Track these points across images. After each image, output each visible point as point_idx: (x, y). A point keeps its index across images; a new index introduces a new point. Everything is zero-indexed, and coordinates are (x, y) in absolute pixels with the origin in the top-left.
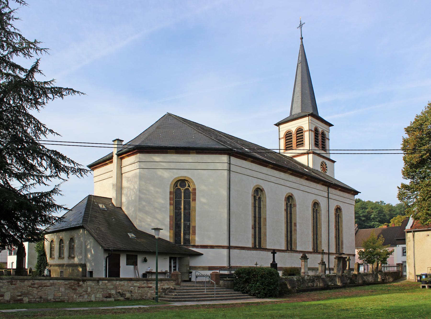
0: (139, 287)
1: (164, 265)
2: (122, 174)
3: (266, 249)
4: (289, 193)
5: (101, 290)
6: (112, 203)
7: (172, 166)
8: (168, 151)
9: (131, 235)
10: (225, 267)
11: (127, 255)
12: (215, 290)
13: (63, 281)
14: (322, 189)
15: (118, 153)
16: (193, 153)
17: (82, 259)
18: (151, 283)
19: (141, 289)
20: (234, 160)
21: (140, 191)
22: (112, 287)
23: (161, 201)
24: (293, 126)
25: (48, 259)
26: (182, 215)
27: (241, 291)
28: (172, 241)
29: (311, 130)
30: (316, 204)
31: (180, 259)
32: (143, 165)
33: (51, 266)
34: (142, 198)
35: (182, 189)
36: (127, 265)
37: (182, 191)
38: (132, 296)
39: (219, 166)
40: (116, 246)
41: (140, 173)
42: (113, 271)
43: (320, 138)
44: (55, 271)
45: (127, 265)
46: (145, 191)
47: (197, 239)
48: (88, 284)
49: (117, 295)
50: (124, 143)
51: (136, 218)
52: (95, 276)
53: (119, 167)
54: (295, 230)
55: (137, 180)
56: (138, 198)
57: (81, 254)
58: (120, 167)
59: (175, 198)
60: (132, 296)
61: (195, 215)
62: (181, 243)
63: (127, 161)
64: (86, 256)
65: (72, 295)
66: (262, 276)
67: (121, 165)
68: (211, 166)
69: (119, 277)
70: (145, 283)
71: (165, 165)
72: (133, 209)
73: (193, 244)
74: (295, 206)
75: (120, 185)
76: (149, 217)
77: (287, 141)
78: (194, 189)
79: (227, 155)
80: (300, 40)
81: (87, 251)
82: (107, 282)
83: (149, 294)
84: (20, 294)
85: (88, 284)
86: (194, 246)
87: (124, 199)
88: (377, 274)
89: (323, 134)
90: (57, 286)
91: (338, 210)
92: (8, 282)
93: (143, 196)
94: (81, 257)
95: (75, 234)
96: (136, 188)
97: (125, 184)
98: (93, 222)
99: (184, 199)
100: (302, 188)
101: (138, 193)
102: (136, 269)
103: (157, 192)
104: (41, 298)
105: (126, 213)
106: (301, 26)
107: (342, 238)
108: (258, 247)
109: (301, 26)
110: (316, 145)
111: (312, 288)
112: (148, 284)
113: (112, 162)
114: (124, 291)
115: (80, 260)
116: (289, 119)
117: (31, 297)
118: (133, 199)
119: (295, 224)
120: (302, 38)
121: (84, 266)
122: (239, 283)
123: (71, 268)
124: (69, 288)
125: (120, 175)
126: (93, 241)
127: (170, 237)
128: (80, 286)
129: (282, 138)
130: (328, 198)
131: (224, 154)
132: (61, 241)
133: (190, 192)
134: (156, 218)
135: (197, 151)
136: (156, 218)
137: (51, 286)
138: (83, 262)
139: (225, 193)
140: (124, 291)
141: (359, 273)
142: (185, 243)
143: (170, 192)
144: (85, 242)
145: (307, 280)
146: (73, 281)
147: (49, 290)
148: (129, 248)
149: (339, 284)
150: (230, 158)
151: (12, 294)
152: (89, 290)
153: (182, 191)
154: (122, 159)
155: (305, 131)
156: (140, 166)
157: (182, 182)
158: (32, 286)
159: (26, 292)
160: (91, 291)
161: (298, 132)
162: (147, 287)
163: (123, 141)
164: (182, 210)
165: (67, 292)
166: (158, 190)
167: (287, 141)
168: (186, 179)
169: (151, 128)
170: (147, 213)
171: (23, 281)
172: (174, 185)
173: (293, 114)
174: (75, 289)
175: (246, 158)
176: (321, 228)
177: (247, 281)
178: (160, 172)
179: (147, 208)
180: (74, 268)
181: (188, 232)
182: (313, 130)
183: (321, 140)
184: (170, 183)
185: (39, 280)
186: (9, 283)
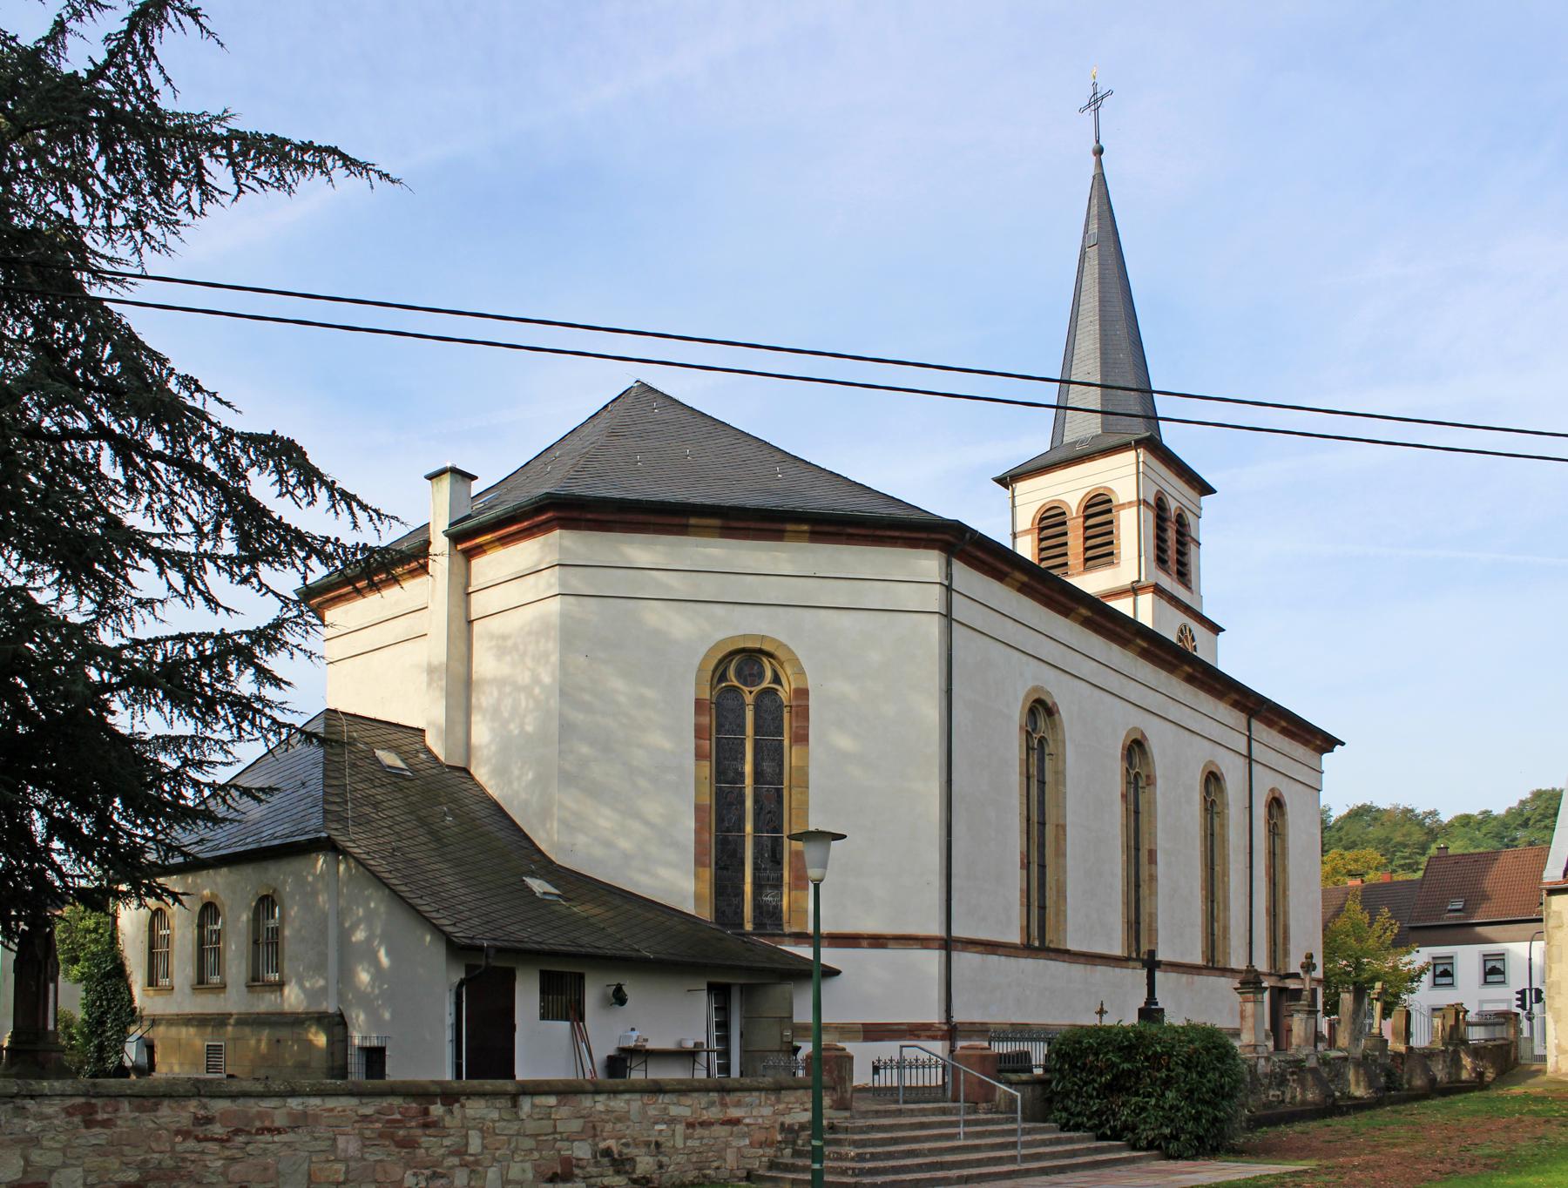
0: (690, 1125)
1: (673, 1018)
2: (470, 622)
3: (1067, 952)
4: (1135, 729)
5: (530, 1143)
6: (428, 751)
7: (709, 587)
8: (693, 521)
9: (538, 886)
10: (931, 1025)
11: (543, 973)
13: (354, 1101)
14: (1231, 723)
15: (459, 527)
16: (798, 536)
17: (324, 990)
18: (738, 1104)
19: (699, 1131)
20: (964, 576)
21: (563, 693)
22: (576, 1125)
23: (658, 739)
24: (1069, 488)
25: (137, 990)
27: (1090, 1129)
28: (706, 914)
29: (1146, 503)
30: (1213, 779)
31: (748, 991)
32: (578, 581)
33: (154, 1022)
34: (573, 727)
36: (543, 1017)
37: (749, 699)
38: (661, 1166)
39: (909, 596)
40: (499, 933)
41: (564, 615)
42: (487, 1049)
43: (1171, 535)
44: (178, 1046)
45: (543, 1017)
46: (587, 697)
48: (469, 1112)
49: (597, 1164)
50: (476, 487)
51: (545, 814)
52: (395, 1072)
53: (460, 590)
54: (1153, 878)
55: (552, 646)
56: (554, 726)
57: (319, 967)
58: (463, 592)
59: (718, 732)
60: (661, 1166)
62: (741, 925)
63: (494, 564)
64: (345, 975)
65: (396, 1172)
66: (1189, 1059)
67: (468, 584)
68: (874, 595)
69: (511, 1075)
70: (712, 1104)
71: (678, 585)
72: (530, 776)
74: (1150, 780)
75: (460, 669)
76: (607, 812)
77: (1045, 544)
78: (802, 693)
79: (941, 549)
81: (347, 956)
82: (552, 1100)
83: (730, 1156)
85: (469, 1112)
87: (481, 733)
88: (1456, 1052)
89: (1180, 521)
90: (321, 1131)
91: (1276, 804)
92: (69, 1112)
93: (578, 717)
94: (321, 982)
95: (282, 876)
96: (547, 679)
97: (485, 663)
98: (368, 822)
99: (756, 733)
100: (1175, 712)
101: (554, 703)
102: (579, 1035)
105: (493, 791)
106: (1096, 102)
107: (1286, 913)
108: (1037, 944)
109: (1096, 102)
110: (1161, 561)
111: (1281, 1109)
112: (724, 1105)
113: (424, 569)
114: (626, 1145)
115: (311, 995)
116: (1044, 462)
118: (529, 728)
119: (1152, 855)
120: (1099, 151)
121: (337, 1024)
122: (1079, 1095)
123: (266, 1033)
124: (381, 1135)
125: (464, 625)
126: (382, 909)
127: (698, 897)
128: (434, 1124)
129: (1026, 532)
130: (1249, 757)
132: (209, 910)
133: (781, 706)
135: (818, 528)
136: (638, 816)
137: (293, 1128)
138: (331, 1007)
139: (931, 713)
140: (626, 1145)
141: (1410, 1049)
142: (758, 924)
143: (699, 703)
144: (341, 915)
145: (1266, 1075)
146: (397, 1101)
147: (285, 1152)
148: (553, 941)
149: (1359, 1091)
150: (949, 564)
151: (90, 1180)
152: (475, 1144)
153: (749, 699)
154: (469, 554)
155: (1123, 506)
156: (562, 583)
157: (745, 662)
158: (199, 1131)
159: (169, 1163)
160: (484, 1147)
161: (1091, 511)
162: (724, 1123)
163: (474, 478)
164: (749, 781)
165: (372, 1158)
167: (1045, 544)
168: (766, 647)
169: (575, 437)
170: (596, 792)
171: (148, 1103)
172: (714, 672)
173: (1067, 440)
174: (409, 1144)
175: (1006, 568)
176: (1225, 874)
177: (1117, 1086)
178: (655, 616)
180: (284, 1033)
182: (1152, 502)
183: (1173, 544)
184: (697, 661)
186: (77, 1119)
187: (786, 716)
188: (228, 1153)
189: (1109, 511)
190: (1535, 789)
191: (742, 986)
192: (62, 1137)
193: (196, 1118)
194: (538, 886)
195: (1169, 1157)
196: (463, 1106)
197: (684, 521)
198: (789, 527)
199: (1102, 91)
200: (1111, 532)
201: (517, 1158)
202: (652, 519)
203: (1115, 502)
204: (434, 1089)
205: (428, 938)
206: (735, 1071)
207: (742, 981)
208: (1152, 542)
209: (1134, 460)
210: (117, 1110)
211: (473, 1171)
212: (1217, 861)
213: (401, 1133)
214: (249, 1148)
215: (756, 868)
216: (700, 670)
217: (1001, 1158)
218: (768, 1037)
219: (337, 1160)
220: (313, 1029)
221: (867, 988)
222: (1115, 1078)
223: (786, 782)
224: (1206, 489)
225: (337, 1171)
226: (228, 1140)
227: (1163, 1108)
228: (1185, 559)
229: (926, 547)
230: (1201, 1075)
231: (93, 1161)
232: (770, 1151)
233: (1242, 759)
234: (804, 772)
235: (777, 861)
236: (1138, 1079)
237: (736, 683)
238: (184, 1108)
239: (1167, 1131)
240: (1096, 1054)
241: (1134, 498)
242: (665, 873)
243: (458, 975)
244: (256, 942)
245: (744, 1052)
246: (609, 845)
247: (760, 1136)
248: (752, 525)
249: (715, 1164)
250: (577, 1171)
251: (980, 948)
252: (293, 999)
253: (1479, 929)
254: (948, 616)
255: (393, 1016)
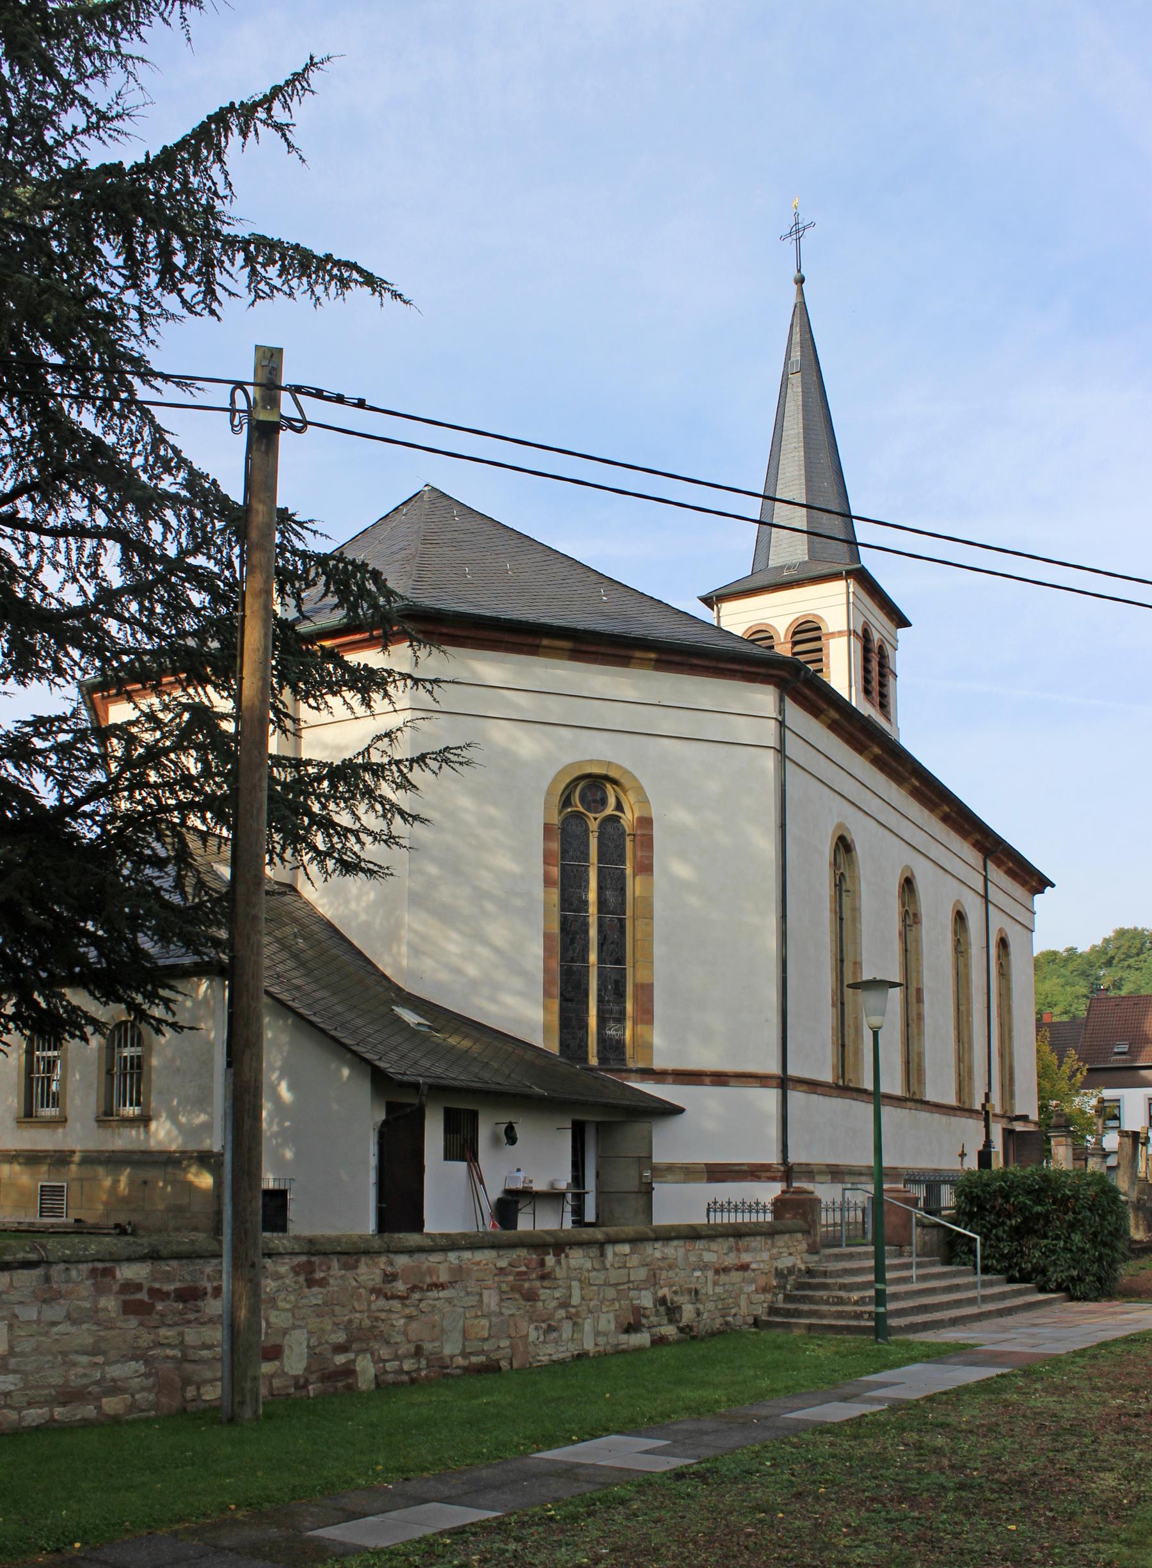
5: (611, 1293)
7: (555, 709)
8: (545, 642)
10: (770, 1165)
12: (914, 1272)
16: (643, 663)
18: (747, 1250)
23: (506, 863)
26: (593, 932)
27: (999, 1272)
28: (554, 1048)
30: (960, 917)
31: (603, 1129)
35: (591, 815)
36: (446, 1159)
37: (593, 826)
39: (744, 730)
43: (874, 666)
47: (658, 1040)
51: (391, 936)
61: (650, 935)
62: (585, 1059)
68: (713, 727)
73: (641, 1065)
76: (454, 935)
78: (646, 822)
79: (777, 685)
80: (795, 287)
82: (626, 1249)
84: (340, 1337)
86: (649, 1073)
91: (1003, 943)
94: (203, 1118)
99: (599, 861)
100: (936, 852)
103: (490, 823)
104: (418, 1352)
106: (797, 231)
109: (797, 231)
115: (188, 1132)
117: (384, 1352)
120: (800, 281)
127: (546, 1028)
130: (985, 897)
131: (765, 679)
133: (623, 834)
134: (486, 943)
135: (664, 657)
136: (486, 943)
139: (767, 847)
140: (675, 1292)
142: (602, 1059)
143: (547, 828)
146: (523, 1252)
148: (458, 1076)
150: (781, 700)
151: (313, 1342)
153: (593, 826)
155: (832, 635)
157: (590, 788)
160: (583, 1298)
164: (593, 909)
166: (492, 811)
168: (612, 774)
170: (446, 915)
174: (531, 1297)
179: (444, 894)
181: (616, 1008)
182: (860, 633)
184: (545, 785)
185: (411, 1251)
187: (629, 844)
188: (407, 1311)
189: (819, 639)
190: (1118, 927)
191: (597, 1123)
192: (292, 1298)
193: (385, 1275)
194: (410, 1017)
195: (1072, 1298)
196: (567, 1256)
197: (537, 642)
198: (638, 654)
199: (804, 220)
200: (821, 660)
201: (605, 1310)
202: (507, 637)
203: (824, 631)
204: (549, 1239)
205: (346, 1072)
206: (590, 1216)
207: (598, 1119)
208: (860, 673)
209: (844, 590)
210: (329, 1268)
211: (575, 1324)
212: (963, 1001)
213: (526, 1285)
214: (423, 1305)
215: (600, 1000)
216: (549, 794)
217: (961, 1301)
218: (626, 1179)
219: (483, 1316)
220: (194, 1169)
221: (718, 1126)
222: (1026, 1220)
223: (629, 913)
224: (902, 621)
225: (483, 1327)
226: (407, 1298)
227: (1071, 1251)
228: (885, 691)
229: (762, 682)
230: (1103, 1217)
231: (313, 1322)
232: (769, 1297)
233: (979, 898)
234: (648, 902)
235: (620, 995)
236: (1048, 1222)
237: (582, 810)
238: (376, 1265)
239: (1075, 1273)
240: (1006, 1198)
241: (845, 628)
242: (510, 1000)
243: (381, 1116)
244: (109, 1072)
245: (600, 1193)
246: (458, 971)
247: (762, 1281)
248: (602, 650)
249: (733, 1311)
250: (644, 1321)
251: (805, 1087)
252: (162, 1134)
253: (1143, 1073)
254: (781, 751)
255: (296, 1154)
